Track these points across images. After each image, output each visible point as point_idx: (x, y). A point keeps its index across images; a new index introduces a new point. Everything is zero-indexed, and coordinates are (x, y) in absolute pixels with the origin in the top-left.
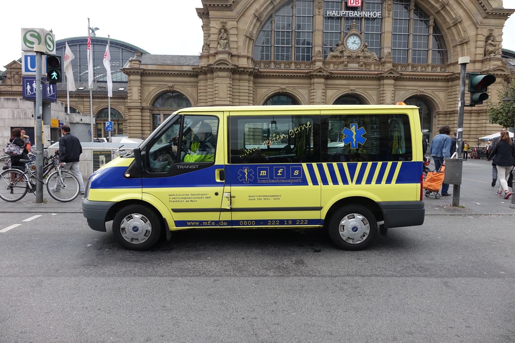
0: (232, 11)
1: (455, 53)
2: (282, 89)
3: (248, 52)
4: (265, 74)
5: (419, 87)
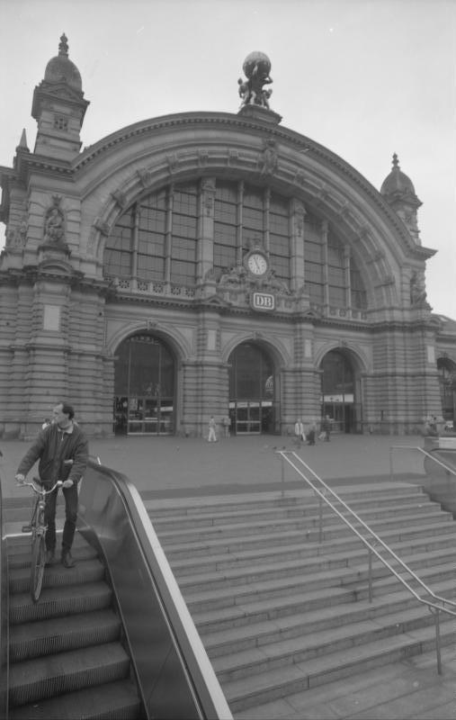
0: (73, 181)
3: (97, 255)
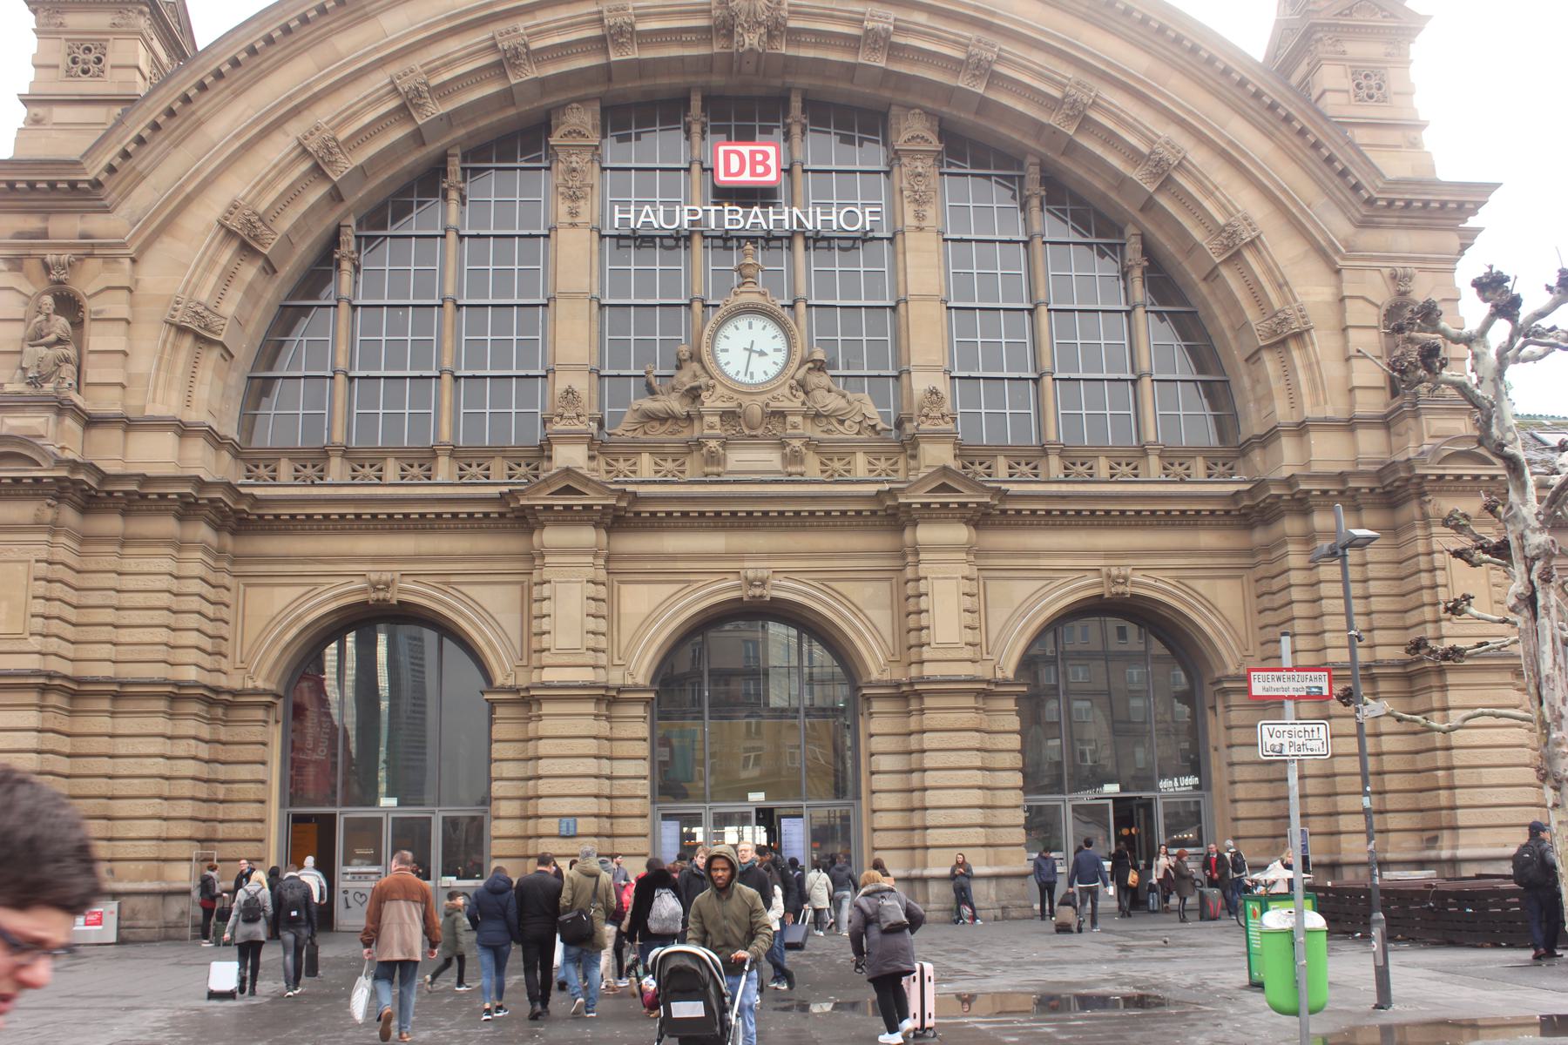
0: (106, 210)
1: (1260, 389)
2: (751, 583)
4: (285, 511)
5: (1109, 554)
